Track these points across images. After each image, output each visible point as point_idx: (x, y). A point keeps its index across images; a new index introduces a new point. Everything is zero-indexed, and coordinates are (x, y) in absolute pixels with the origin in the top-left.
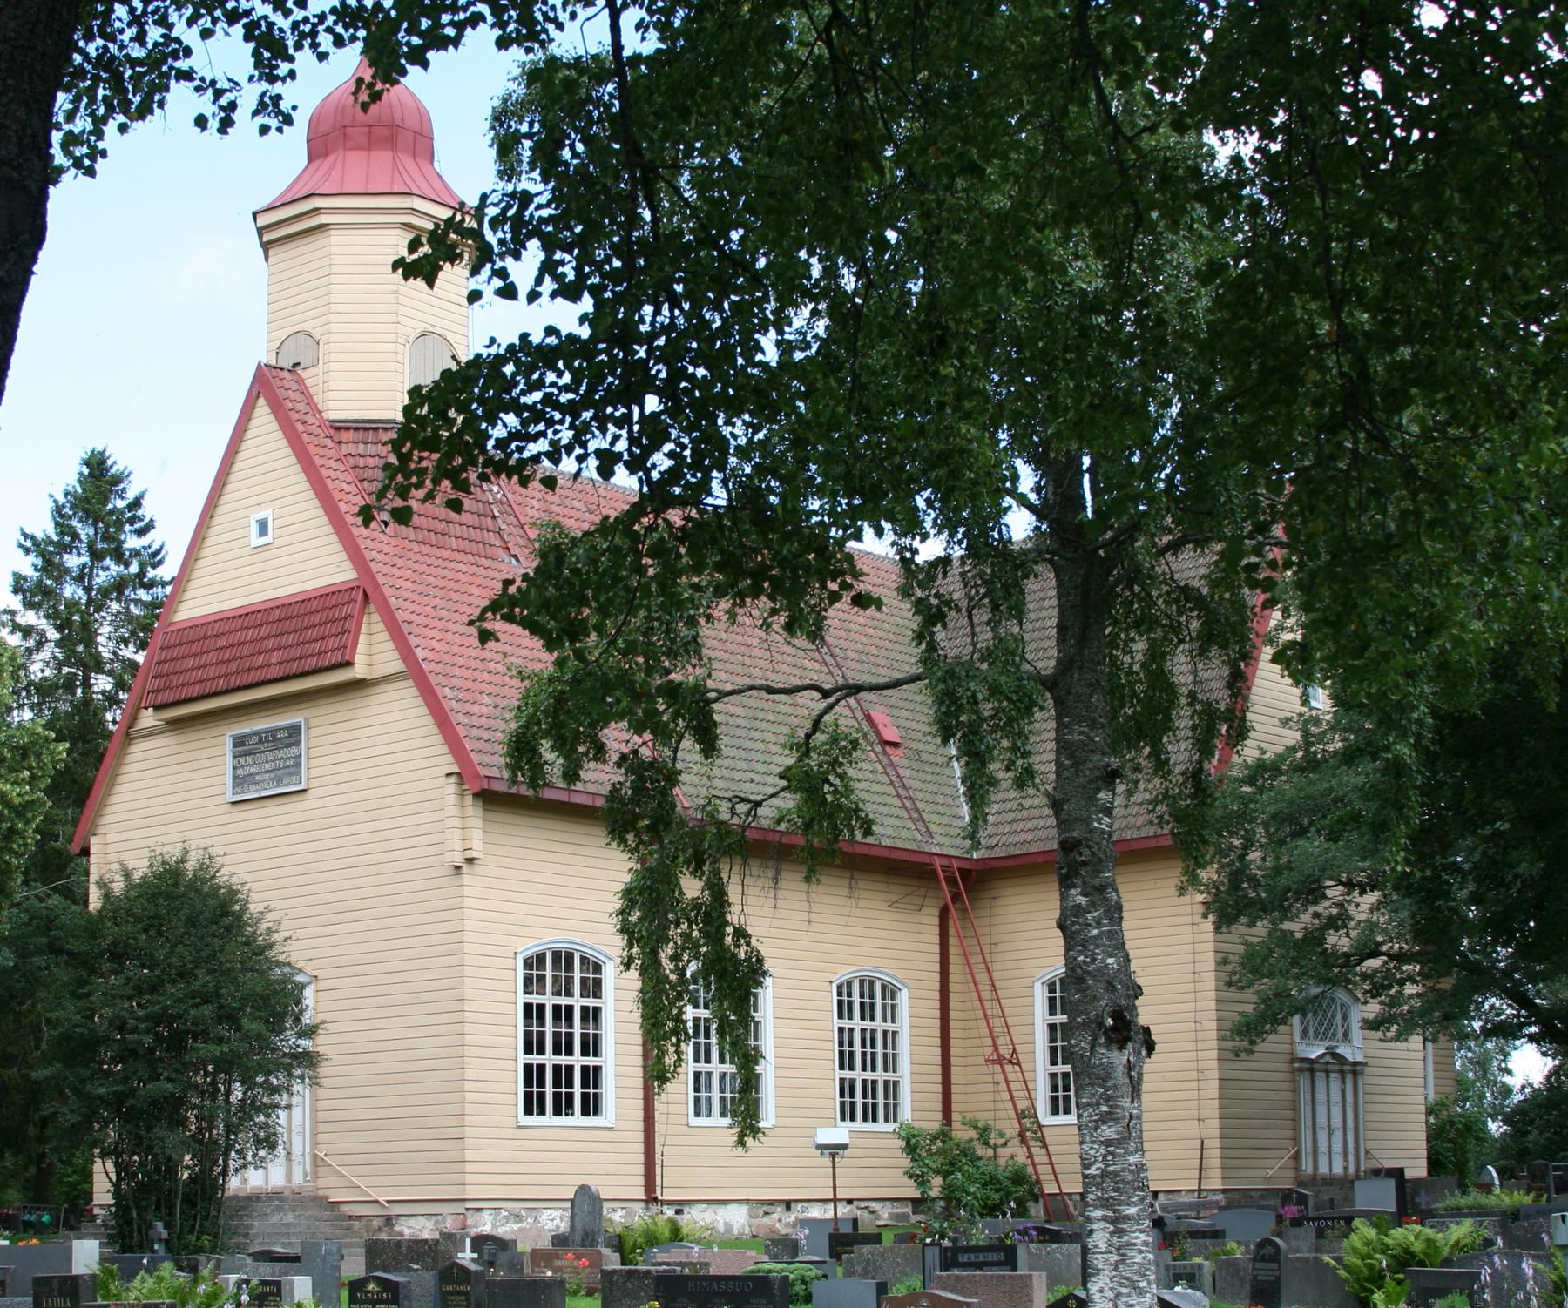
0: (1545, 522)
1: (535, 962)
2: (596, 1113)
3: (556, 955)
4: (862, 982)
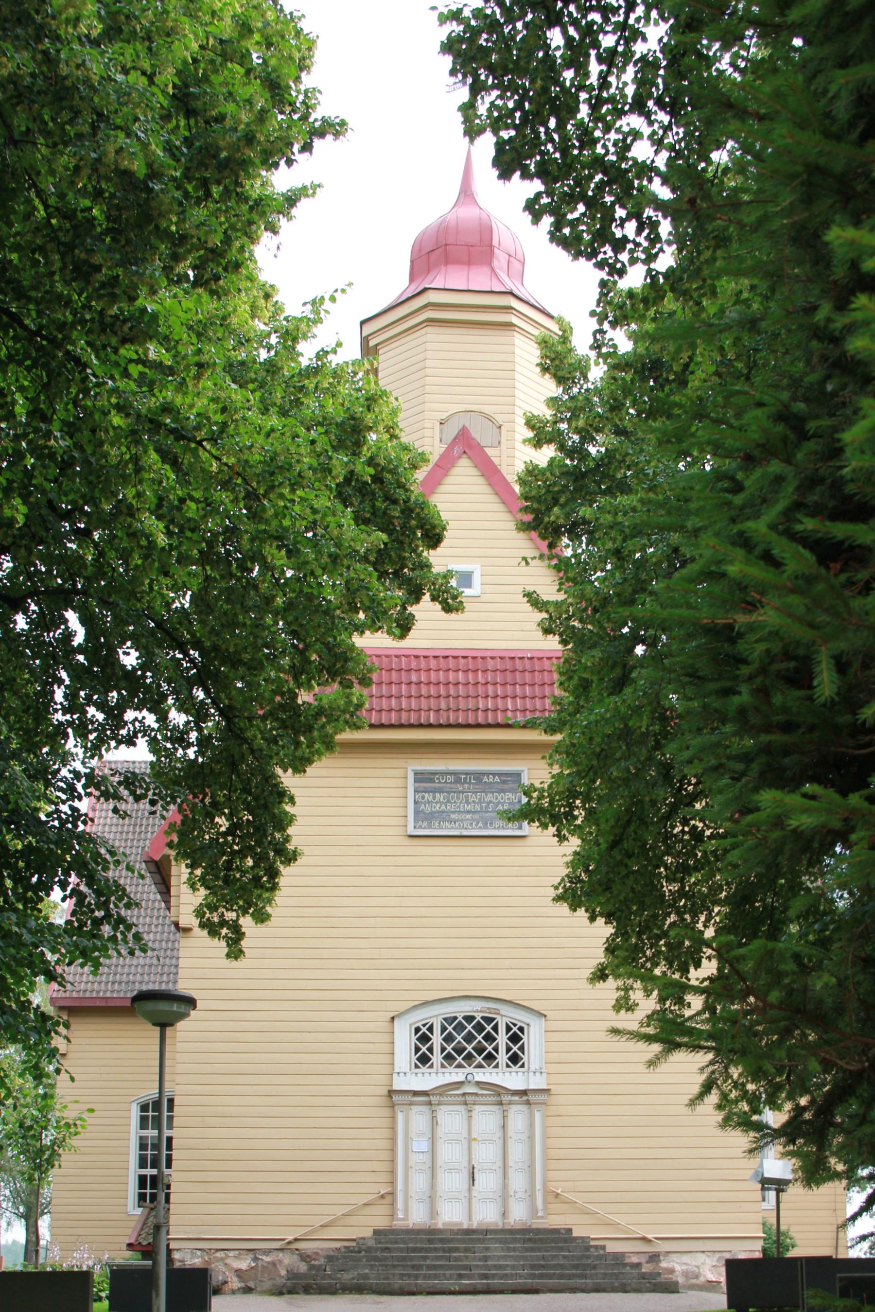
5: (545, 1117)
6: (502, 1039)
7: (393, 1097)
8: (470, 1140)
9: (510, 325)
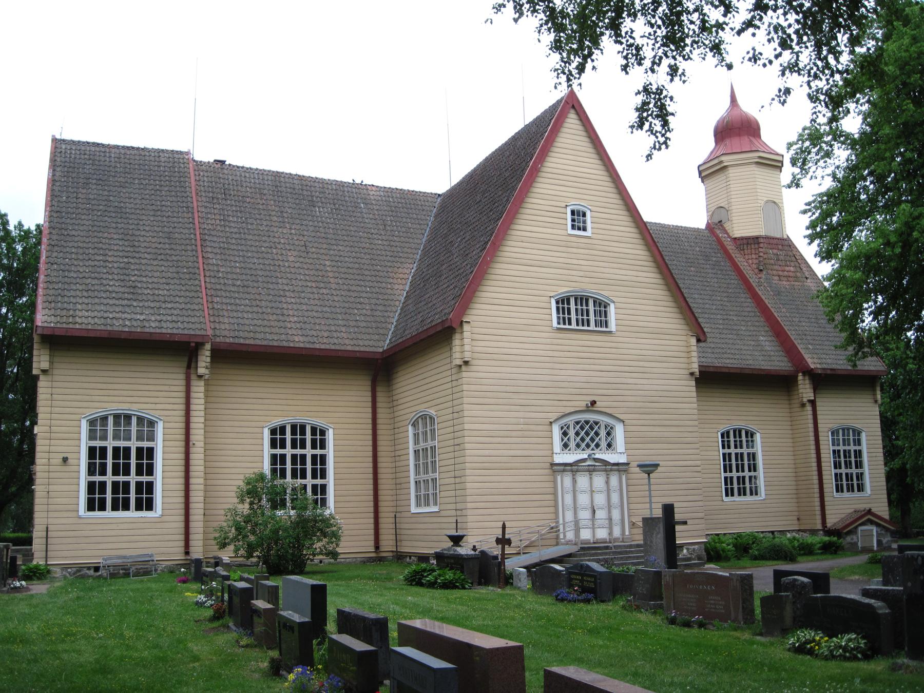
0: (647, 63)
1: (725, 435)
2: (151, 509)
3: (294, 427)
4: (735, 431)
5: (627, 479)
6: (603, 433)
7: (558, 469)
8: (592, 491)
9: (726, 167)
